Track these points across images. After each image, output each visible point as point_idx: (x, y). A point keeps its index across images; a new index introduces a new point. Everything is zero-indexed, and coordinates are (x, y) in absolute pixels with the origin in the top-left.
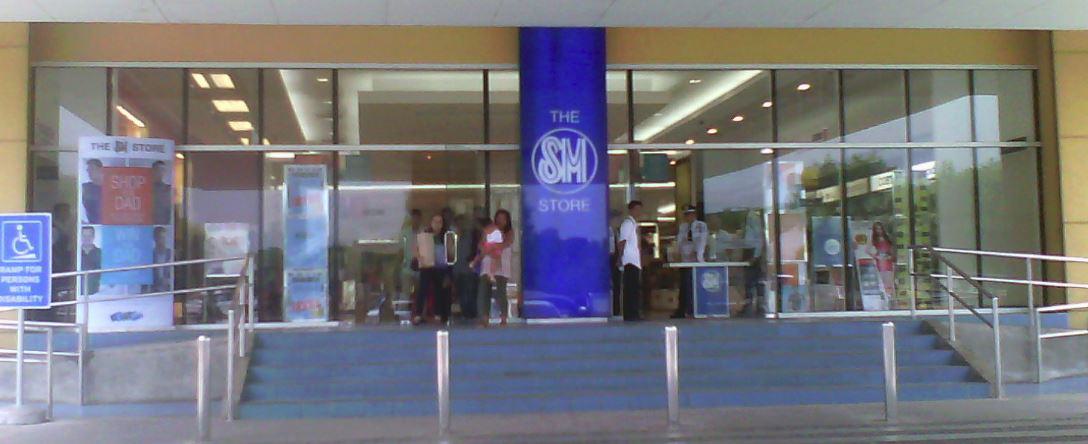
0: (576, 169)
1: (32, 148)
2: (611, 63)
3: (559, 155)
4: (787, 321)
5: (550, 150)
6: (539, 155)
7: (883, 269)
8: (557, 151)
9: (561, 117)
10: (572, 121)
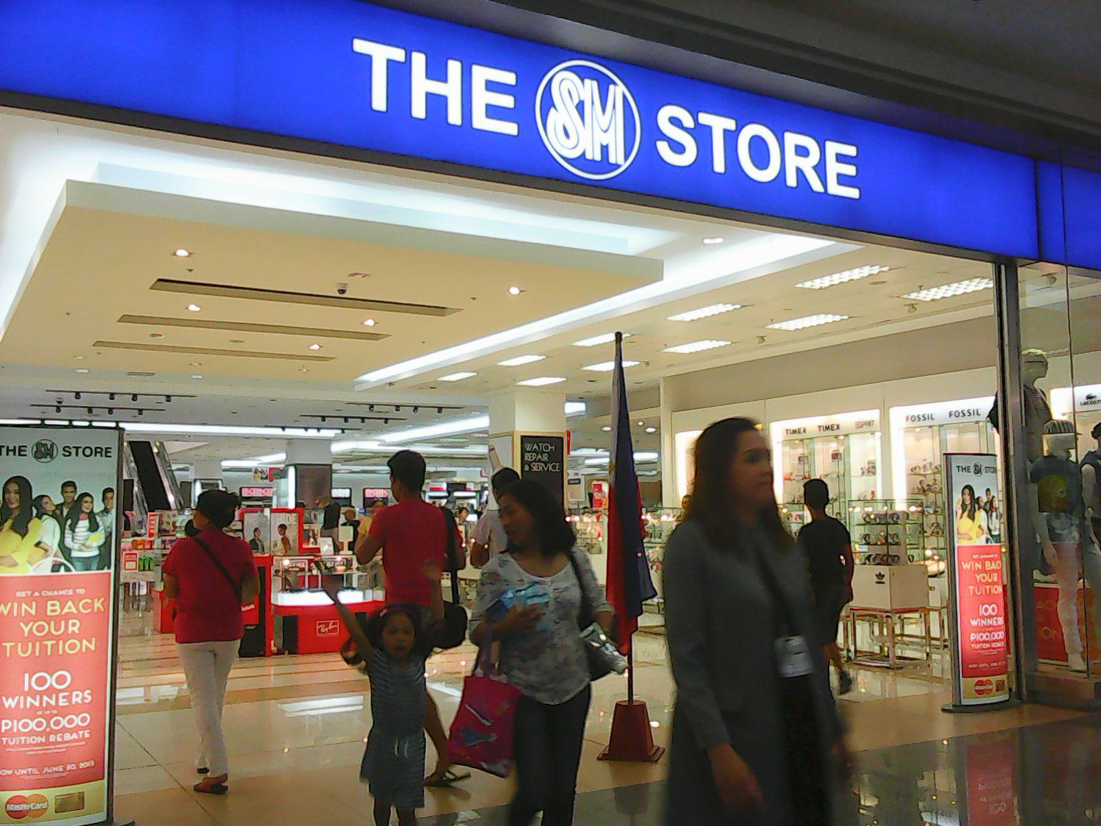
0: (606, 139)
1: (29, 451)
2: (287, 503)
3: (580, 107)
4: (289, 609)
5: (566, 95)
6: (548, 103)
7: (443, 674)
8: (576, 101)
9: (421, 86)
10: (481, 121)
